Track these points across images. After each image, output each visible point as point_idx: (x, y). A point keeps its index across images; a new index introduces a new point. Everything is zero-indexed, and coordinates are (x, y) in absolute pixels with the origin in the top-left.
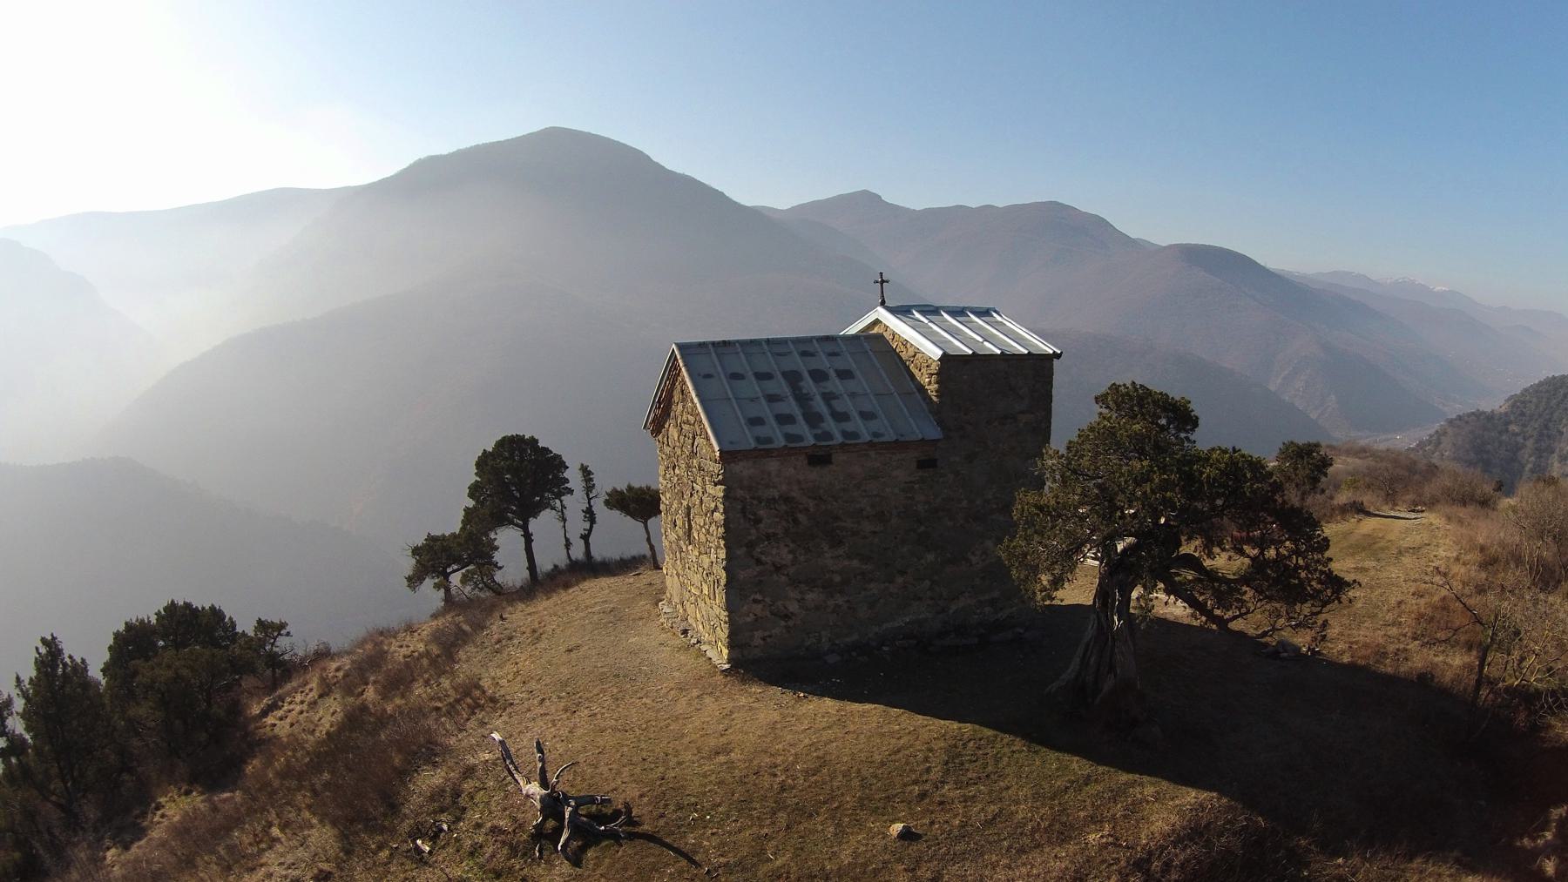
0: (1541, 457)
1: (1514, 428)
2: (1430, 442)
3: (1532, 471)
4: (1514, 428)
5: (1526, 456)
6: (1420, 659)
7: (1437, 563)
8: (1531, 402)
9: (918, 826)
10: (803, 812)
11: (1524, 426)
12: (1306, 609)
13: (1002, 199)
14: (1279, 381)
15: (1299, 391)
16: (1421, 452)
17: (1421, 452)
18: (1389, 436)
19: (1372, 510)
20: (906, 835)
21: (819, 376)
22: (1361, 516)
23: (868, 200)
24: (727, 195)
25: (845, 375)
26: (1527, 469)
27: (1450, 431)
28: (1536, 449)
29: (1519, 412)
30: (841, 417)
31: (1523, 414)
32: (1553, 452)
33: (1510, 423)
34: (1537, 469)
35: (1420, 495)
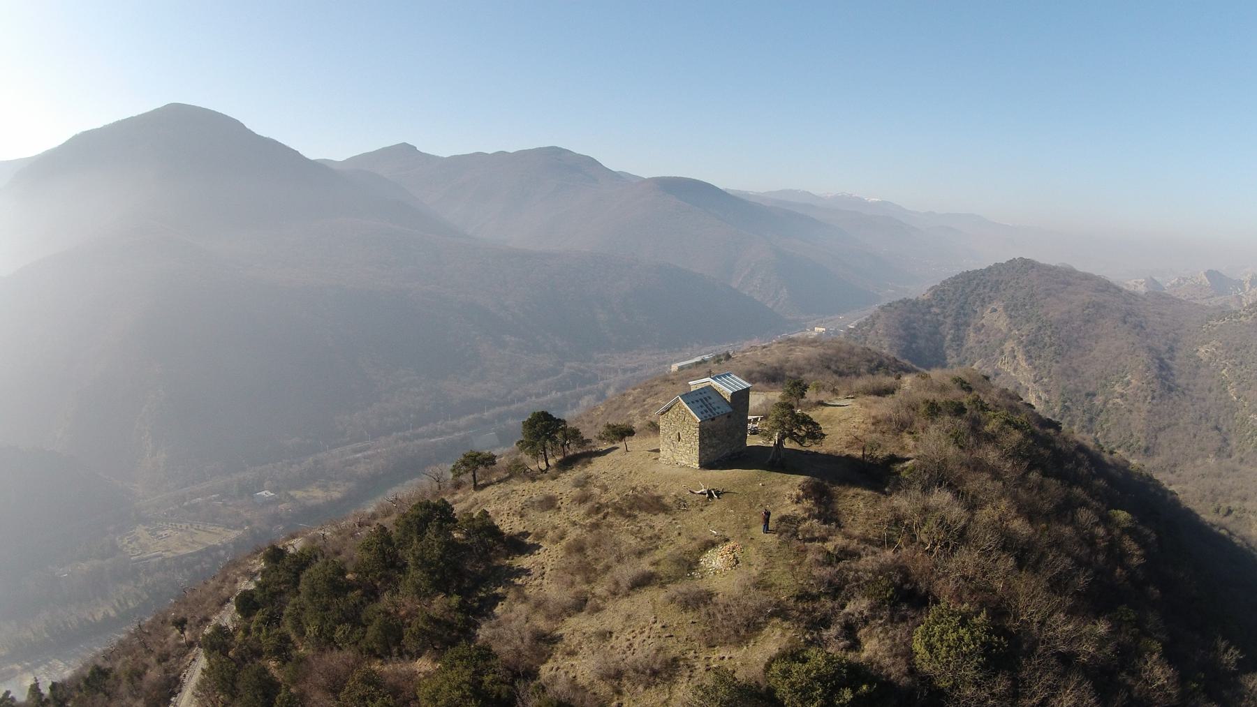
1: (934, 310)
2: (866, 324)
3: (952, 340)
4: (934, 310)
5: (947, 329)
6: (847, 452)
7: (854, 424)
11: (944, 308)
12: (818, 440)
13: (513, 146)
15: (757, 287)
16: (859, 331)
17: (859, 331)
18: (832, 317)
19: (826, 402)
22: (823, 407)
23: (406, 151)
24: (259, 134)
26: (947, 339)
28: (955, 324)
29: (939, 299)
31: (942, 300)
33: (932, 306)
34: (956, 338)
35: (851, 389)
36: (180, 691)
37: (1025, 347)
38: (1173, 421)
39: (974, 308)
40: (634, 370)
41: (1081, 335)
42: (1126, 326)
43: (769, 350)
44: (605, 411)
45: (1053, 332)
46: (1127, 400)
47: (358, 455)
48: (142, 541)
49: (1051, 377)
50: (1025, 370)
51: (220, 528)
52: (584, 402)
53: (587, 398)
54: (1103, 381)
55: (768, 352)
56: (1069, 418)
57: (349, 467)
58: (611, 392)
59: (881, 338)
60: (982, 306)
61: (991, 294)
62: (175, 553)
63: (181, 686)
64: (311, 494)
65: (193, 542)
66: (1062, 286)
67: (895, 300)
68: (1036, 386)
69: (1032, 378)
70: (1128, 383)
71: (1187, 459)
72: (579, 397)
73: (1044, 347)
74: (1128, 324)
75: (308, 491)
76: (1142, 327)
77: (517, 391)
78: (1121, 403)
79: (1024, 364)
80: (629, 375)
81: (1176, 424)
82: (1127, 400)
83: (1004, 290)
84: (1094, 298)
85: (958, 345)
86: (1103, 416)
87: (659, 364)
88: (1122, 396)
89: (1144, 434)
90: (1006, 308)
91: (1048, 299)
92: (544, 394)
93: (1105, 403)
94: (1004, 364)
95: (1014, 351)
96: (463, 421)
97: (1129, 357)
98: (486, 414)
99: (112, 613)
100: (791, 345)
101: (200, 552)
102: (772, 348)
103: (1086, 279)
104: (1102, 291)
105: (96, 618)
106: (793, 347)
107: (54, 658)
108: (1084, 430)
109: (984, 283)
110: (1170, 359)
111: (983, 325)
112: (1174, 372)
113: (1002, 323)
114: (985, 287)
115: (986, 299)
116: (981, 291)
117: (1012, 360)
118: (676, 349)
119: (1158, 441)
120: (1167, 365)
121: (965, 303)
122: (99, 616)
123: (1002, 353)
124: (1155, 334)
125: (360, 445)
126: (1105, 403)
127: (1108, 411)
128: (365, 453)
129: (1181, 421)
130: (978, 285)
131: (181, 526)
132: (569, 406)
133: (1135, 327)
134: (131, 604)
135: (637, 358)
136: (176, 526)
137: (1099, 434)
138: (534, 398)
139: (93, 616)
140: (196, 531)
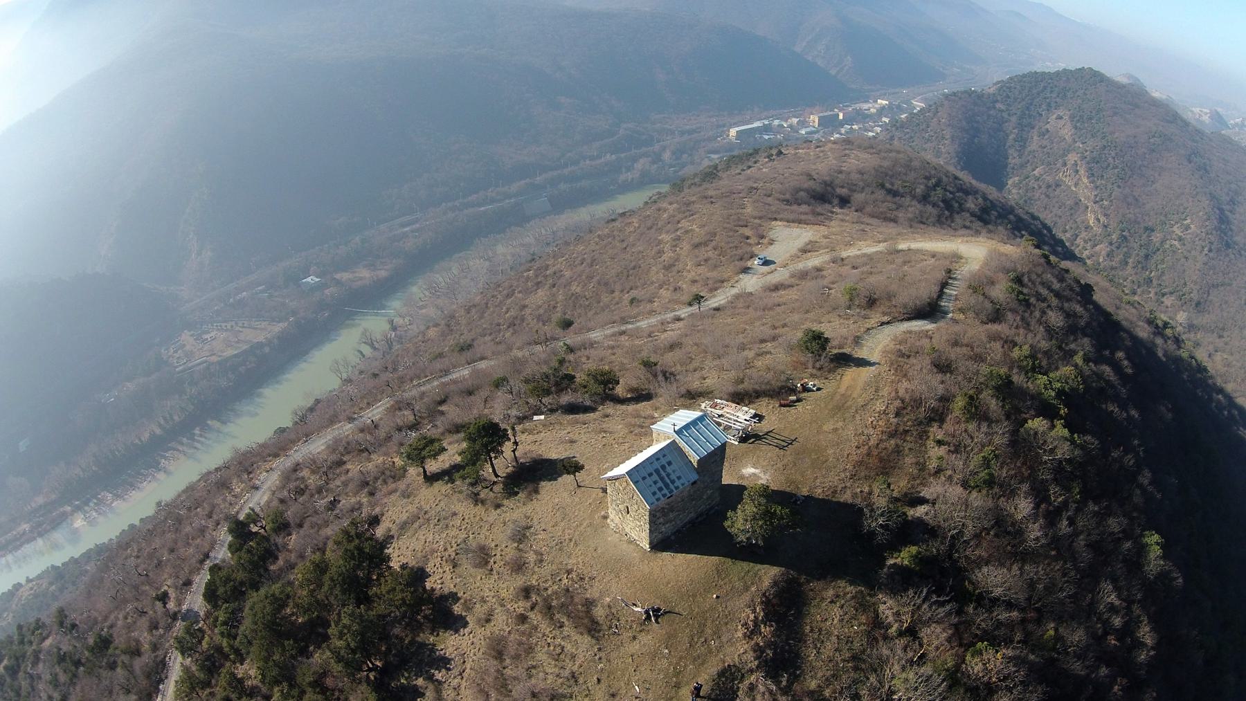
0: (1023, 130)
1: (998, 105)
4: (998, 105)
5: (1011, 128)
8: (1015, 88)
9: (718, 593)
10: (694, 596)
14: (804, 44)
17: (922, 117)
18: (897, 90)
20: (717, 597)
21: (663, 467)
25: (670, 463)
26: (1010, 137)
27: (946, 103)
28: (1019, 124)
30: (673, 482)
31: (1008, 97)
32: (1033, 128)
33: (997, 101)
36: (166, 678)
37: (1088, 163)
38: (1227, 281)
39: (1040, 110)
40: (690, 132)
41: (1145, 163)
42: (1190, 166)
43: (822, 152)
44: (639, 227)
45: (1116, 154)
46: (1184, 245)
47: (406, 229)
48: (188, 348)
49: (1111, 201)
50: (1087, 187)
51: (265, 323)
52: (639, 166)
53: (641, 161)
54: (1163, 218)
55: (821, 154)
56: (1125, 249)
57: (396, 244)
58: (667, 156)
59: (943, 127)
60: (1048, 110)
61: (1058, 100)
62: (220, 356)
63: (167, 671)
64: (357, 275)
65: (238, 342)
66: (1131, 107)
67: (959, 90)
68: (1096, 207)
69: (1093, 197)
70: (1188, 228)
71: (1235, 326)
72: (635, 160)
73: (1107, 168)
74: (1192, 164)
75: (354, 272)
76: (1205, 170)
77: (569, 154)
78: (1179, 247)
79: (1085, 180)
80: (686, 137)
81: (1230, 285)
82: (1184, 245)
83: (1071, 98)
84: (1161, 128)
85: (1021, 146)
86: (1158, 257)
87: (718, 126)
88: (1180, 239)
89: (1198, 287)
90: (1072, 118)
91: (1115, 118)
92: (599, 157)
93: (1163, 242)
94: (1066, 176)
95: (1077, 165)
96: (515, 187)
97: (1191, 199)
98: (538, 178)
99: (158, 431)
100: (845, 149)
101: (245, 352)
102: (827, 148)
103: (1154, 105)
104: (1168, 122)
105: (143, 439)
106: (847, 152)
107: (103, 491)
108: (1140, 266)
109: (1052, 88)
110: (1231, 212)
111: (1048, 131)
112: (1233, 228)
113: (1067, 132)
114: (1051, 92)
115: (1053, 105)
116: (1048, 95)
117: (1073, 174)
118: (736, 112)
119: (1210, 298)
120: (1227, 217)
121: (1031, 104)
122: (146, 436)
123: (1065, 164)
124: (1218, 181)
125: (408, 218)
126: (1163, 242)
127: (1164, 252)
128: (414, 226)
129: (1234, 282)
130: (1045, 88)
131: (226, 326)
132: (624, 170)
133: (1199, 169)
134: (176, 418)
135: (695, 120)
136: (221, 326)
137: (1153, 274)
138: (588, 162)
139: (140, 439)
140: (241, 329)
